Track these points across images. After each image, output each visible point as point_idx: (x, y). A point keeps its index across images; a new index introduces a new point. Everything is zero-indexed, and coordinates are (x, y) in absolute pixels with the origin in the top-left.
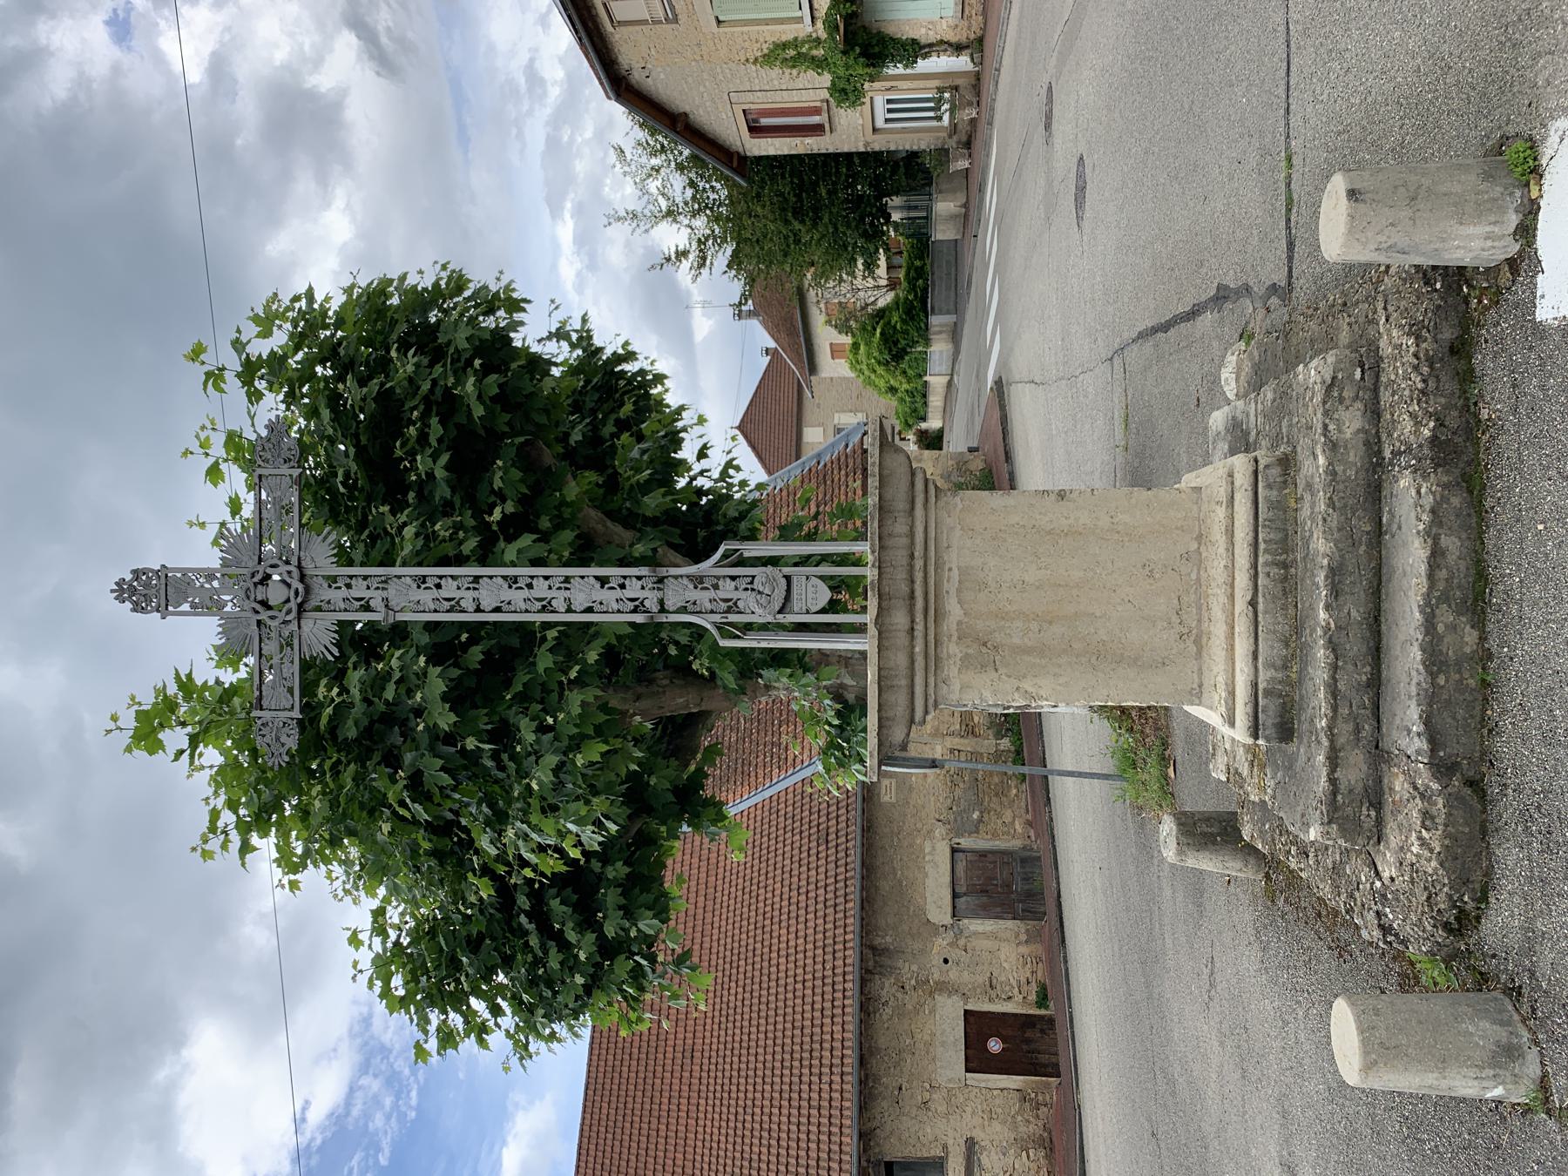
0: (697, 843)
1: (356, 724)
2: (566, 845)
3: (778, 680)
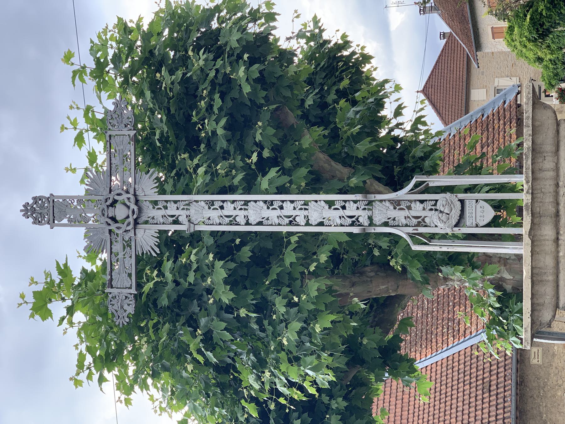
0: (394, 387)
1: (168, 297)
2: (306, 385)
3: (453, 274)
